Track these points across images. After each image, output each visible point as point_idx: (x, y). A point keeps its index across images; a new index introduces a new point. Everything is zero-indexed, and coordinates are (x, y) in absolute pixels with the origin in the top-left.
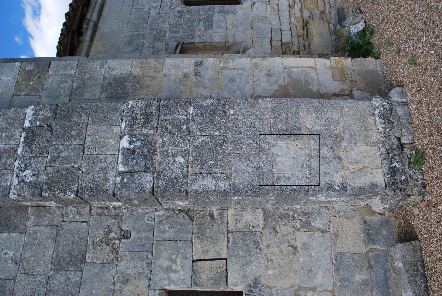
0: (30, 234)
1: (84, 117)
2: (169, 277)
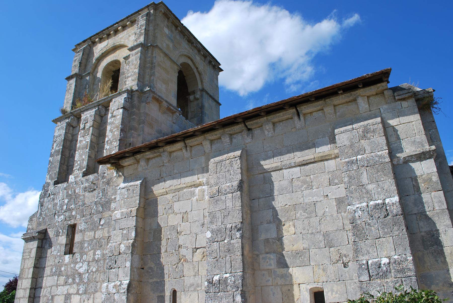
0: (338, 216)
1: (397, 233)
2: (329, 292)
